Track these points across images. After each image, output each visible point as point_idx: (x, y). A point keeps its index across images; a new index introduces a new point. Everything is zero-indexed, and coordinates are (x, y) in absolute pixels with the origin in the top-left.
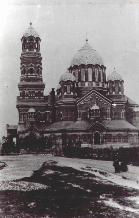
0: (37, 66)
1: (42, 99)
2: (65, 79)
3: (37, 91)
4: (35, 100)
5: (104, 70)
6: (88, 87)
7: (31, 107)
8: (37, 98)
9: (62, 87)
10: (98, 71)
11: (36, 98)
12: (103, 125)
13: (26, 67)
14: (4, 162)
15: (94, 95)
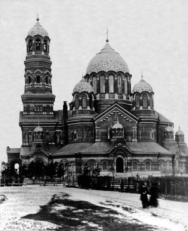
2: (80, 89)
5: (128, 79)
6: (109, 100)
7: (37, 125)
9: (76, 99)
11: (43, 113)
13: (32, 73)
15: (116, 110)
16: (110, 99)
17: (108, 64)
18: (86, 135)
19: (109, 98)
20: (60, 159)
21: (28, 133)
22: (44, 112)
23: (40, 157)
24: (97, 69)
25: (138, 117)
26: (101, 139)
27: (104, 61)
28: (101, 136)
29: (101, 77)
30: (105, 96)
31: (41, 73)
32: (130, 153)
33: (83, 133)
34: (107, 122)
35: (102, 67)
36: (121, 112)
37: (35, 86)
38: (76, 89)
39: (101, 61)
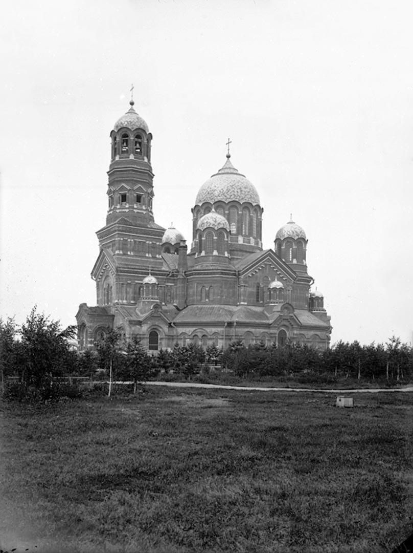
0: (136, 188)
2: (216, 224)
4: (146, 259)
5: (259, 215)
6: (243, 245)
7: (148, 274)
8: (132, 254)
9: (207, 239)
11: (147, 255)
13: (130, 190)
16: (244, 244)
17: (241, 191)
18: (226, 295)
19: (244, 242)
20: (192, 329)
21: (127, 284)
24: (226, 196)
26: (248, 303)
27: (236, 187)
29: (231, 211)
30: (238, 238)
32: (298, 325)
33: (222, 292)
34: (257, 277)
35: (234, 194)
37: (118, 211)
38: (209, 224)
39: (232, 186)
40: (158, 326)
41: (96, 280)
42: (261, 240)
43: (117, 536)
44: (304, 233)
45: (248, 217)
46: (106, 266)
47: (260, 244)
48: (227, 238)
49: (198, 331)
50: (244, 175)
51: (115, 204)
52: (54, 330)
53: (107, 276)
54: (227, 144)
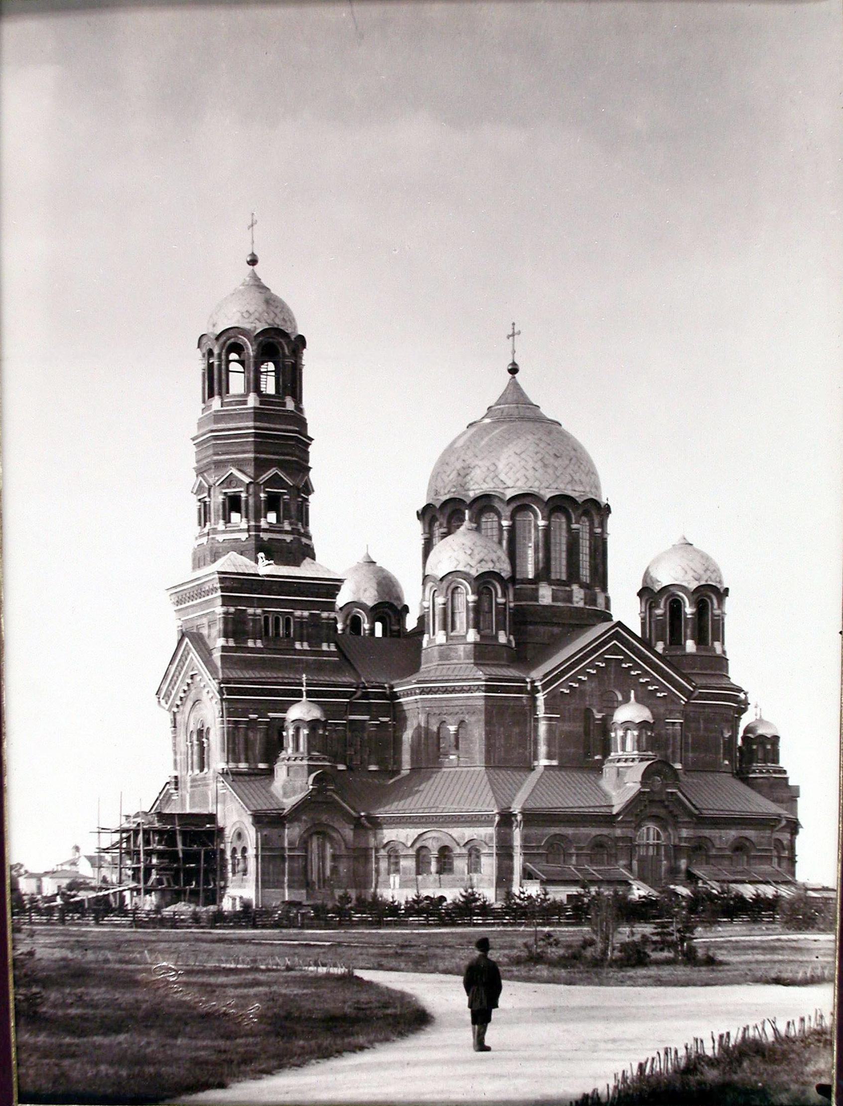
1: (329, 654)
3: (306, 613)
8: (259, 644)
10: (569, 530)
11: (298, 646)
12: (680, 794)
14: (141, 933)
15: (615, 650)
20: (414, 832)
22: (302, 641)
23: (324, 818)
25: (689, 682)
28: (560, 748)
30: (537, 590)
31: (283, 485)
32: (691, 814)
34: (583, 694)
36: (631, 660)
40: (328, 826)
41: (169, 710)
42: (604, 589)
43: (445, 472)
44: (716, 570)
45: (564, 533)
46: (192, 677)
47: (601, 600)
48: (504, 595)
49: (428, 835)
50: (560, 422)
51: (213, 521)
52: (804, 1032)
53: (197, 701)
54: (508, 337)
